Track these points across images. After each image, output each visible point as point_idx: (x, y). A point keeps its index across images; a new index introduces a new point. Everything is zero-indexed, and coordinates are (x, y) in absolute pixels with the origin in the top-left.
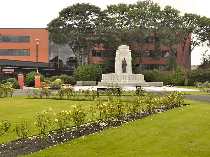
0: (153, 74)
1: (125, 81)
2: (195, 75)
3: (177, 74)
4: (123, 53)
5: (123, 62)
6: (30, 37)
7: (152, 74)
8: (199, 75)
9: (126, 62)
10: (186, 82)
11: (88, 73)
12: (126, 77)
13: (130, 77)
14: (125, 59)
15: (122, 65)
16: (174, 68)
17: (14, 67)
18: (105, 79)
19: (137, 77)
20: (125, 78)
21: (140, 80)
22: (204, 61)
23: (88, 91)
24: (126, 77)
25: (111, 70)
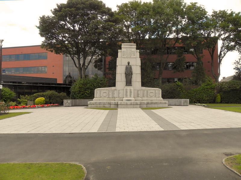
0: (175, 88)
1: (129, 99)
2: (230, 88)
3: (207, 88)
4: (129, 57)
5: (127, 68)
7: (174, 88)
8: (235, 88)
9: (131, 68)
10: (219, 98)
11: (88, 88)
12: (131, 92)
13: (139, 92)
14: (129, 63)
15: (126, 73)
16: (202, 81)
18: (99, 97)
19: (149, 92)
20: (128, 94)
24: (131, 92)
25: (112, 83)
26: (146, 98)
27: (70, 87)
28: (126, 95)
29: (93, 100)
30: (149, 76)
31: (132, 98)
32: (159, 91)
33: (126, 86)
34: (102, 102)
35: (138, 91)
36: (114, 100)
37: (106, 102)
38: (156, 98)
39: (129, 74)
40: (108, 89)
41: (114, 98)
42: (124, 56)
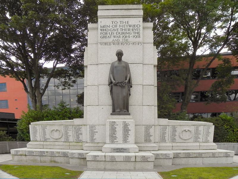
5: (113, 69)
6: (7, 85)
9: (126, 68)
14: (120, 55)
17: (8, 121)
19: (179, 130)
20: (119, 133)
21: (192, 140)
22: (197, 116)
23: (60, 152)
24: (126, 130)
26: (171, 145)
27: (16, 123)
28: (113, 138)
29: (26, 147)
30: (164, 106)
31: (131, 145)
32: (209, 127)
33: (111, 114)
34: (47, 152)
35: (148, 128)
36: (79, 148)
37: (59, 153)
38: (198, 144)
39: (120, 85)
40: (64, 124)
41: (80, 144)
42: (105, 40)
